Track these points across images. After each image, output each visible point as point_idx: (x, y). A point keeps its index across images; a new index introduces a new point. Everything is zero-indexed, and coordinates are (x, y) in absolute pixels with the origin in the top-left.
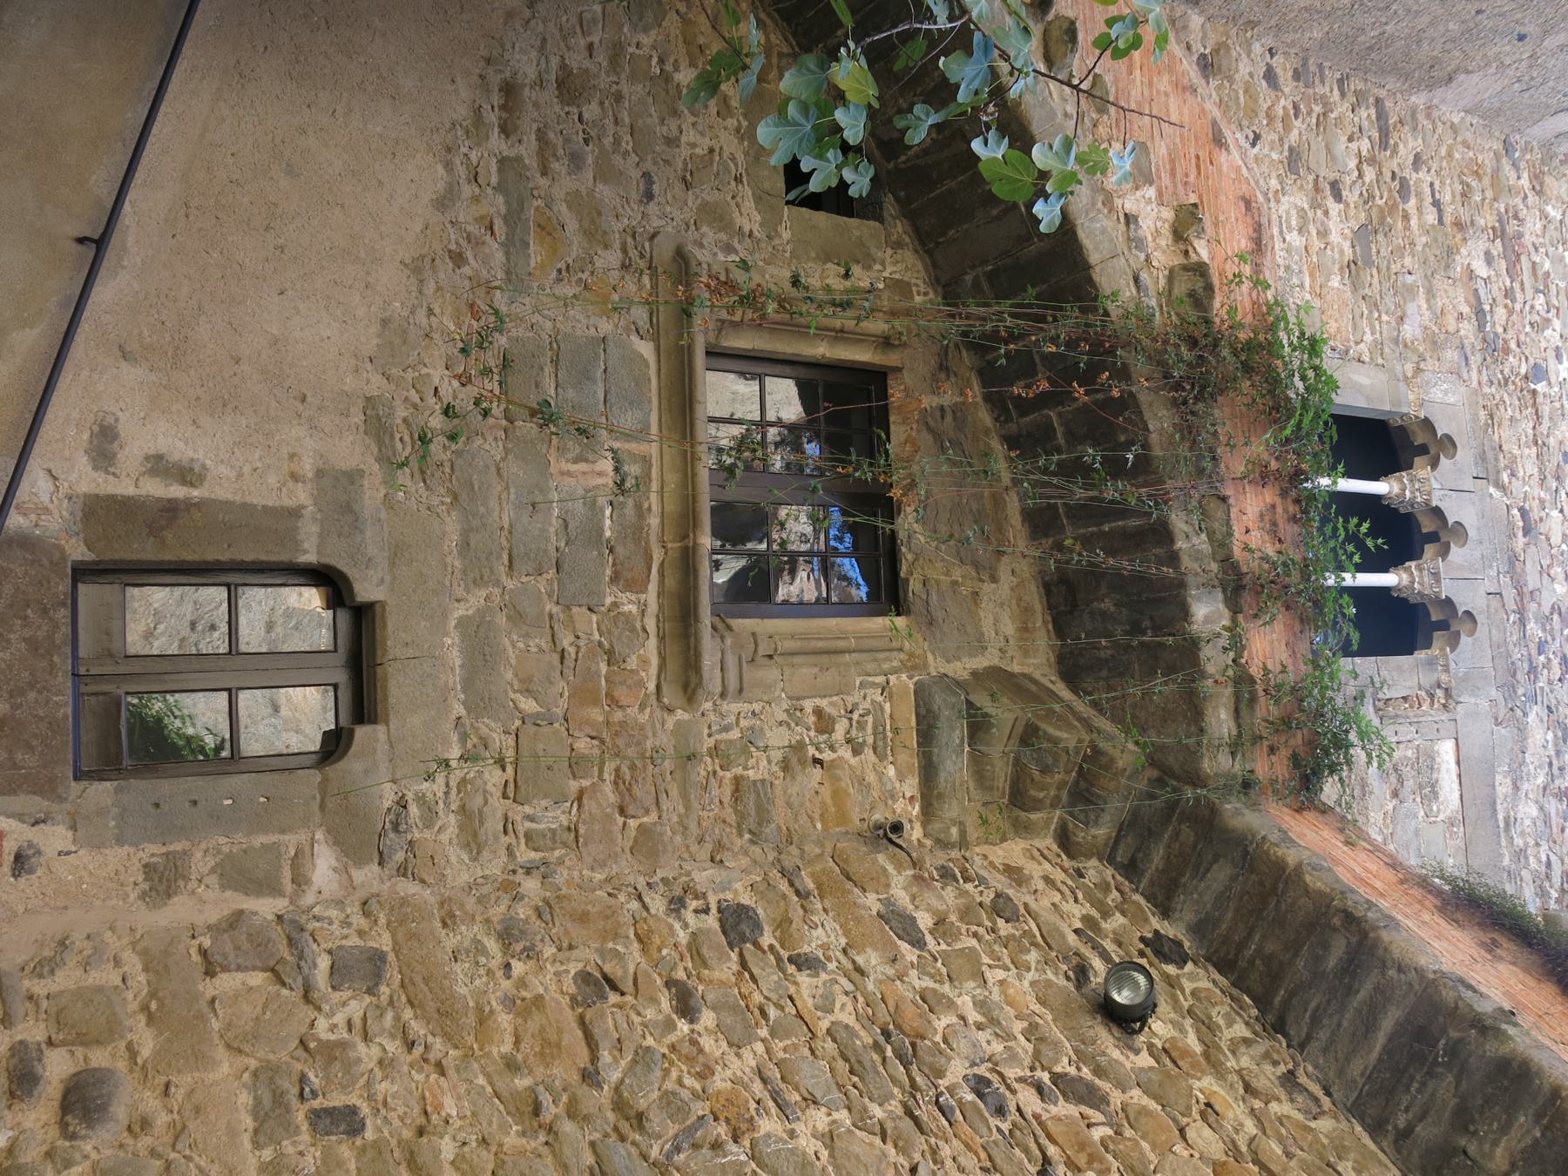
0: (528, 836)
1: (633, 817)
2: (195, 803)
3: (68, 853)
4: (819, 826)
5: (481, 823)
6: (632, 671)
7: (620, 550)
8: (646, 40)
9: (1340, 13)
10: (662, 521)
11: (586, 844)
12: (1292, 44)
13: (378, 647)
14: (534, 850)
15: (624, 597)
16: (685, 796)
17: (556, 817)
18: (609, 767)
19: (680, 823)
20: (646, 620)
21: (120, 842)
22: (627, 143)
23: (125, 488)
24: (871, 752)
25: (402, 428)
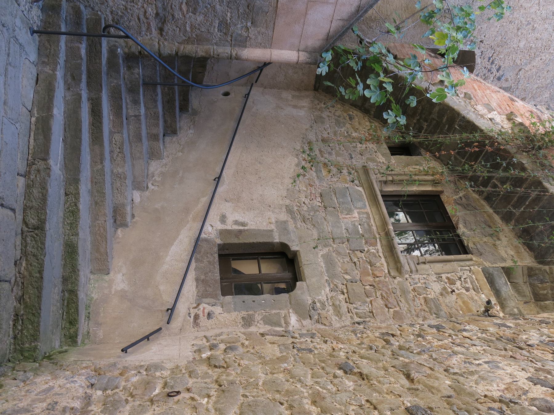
0: (356, 314)
1: (391, 308)
2: (254, 301)
3: (222, 314)
4: (461, 312)
5: (340, 308)
6: (379, 267)
7: (366, 236)
8: (343, 130)
9: (549, 85)
10: (377, 227)
11: (377, 315)
12: (541, 102)
13: (299, 262)
14: (360, 318)
15: (371, 248)
16: (407, 302)
17: (365, 309)
18: (378, 294)
19: (408, 310)
20: (379, 254)
21: (235, 311)
22: (342, 148)
23: (229, 228)
24: (473, 290)
25: (297, 211)
